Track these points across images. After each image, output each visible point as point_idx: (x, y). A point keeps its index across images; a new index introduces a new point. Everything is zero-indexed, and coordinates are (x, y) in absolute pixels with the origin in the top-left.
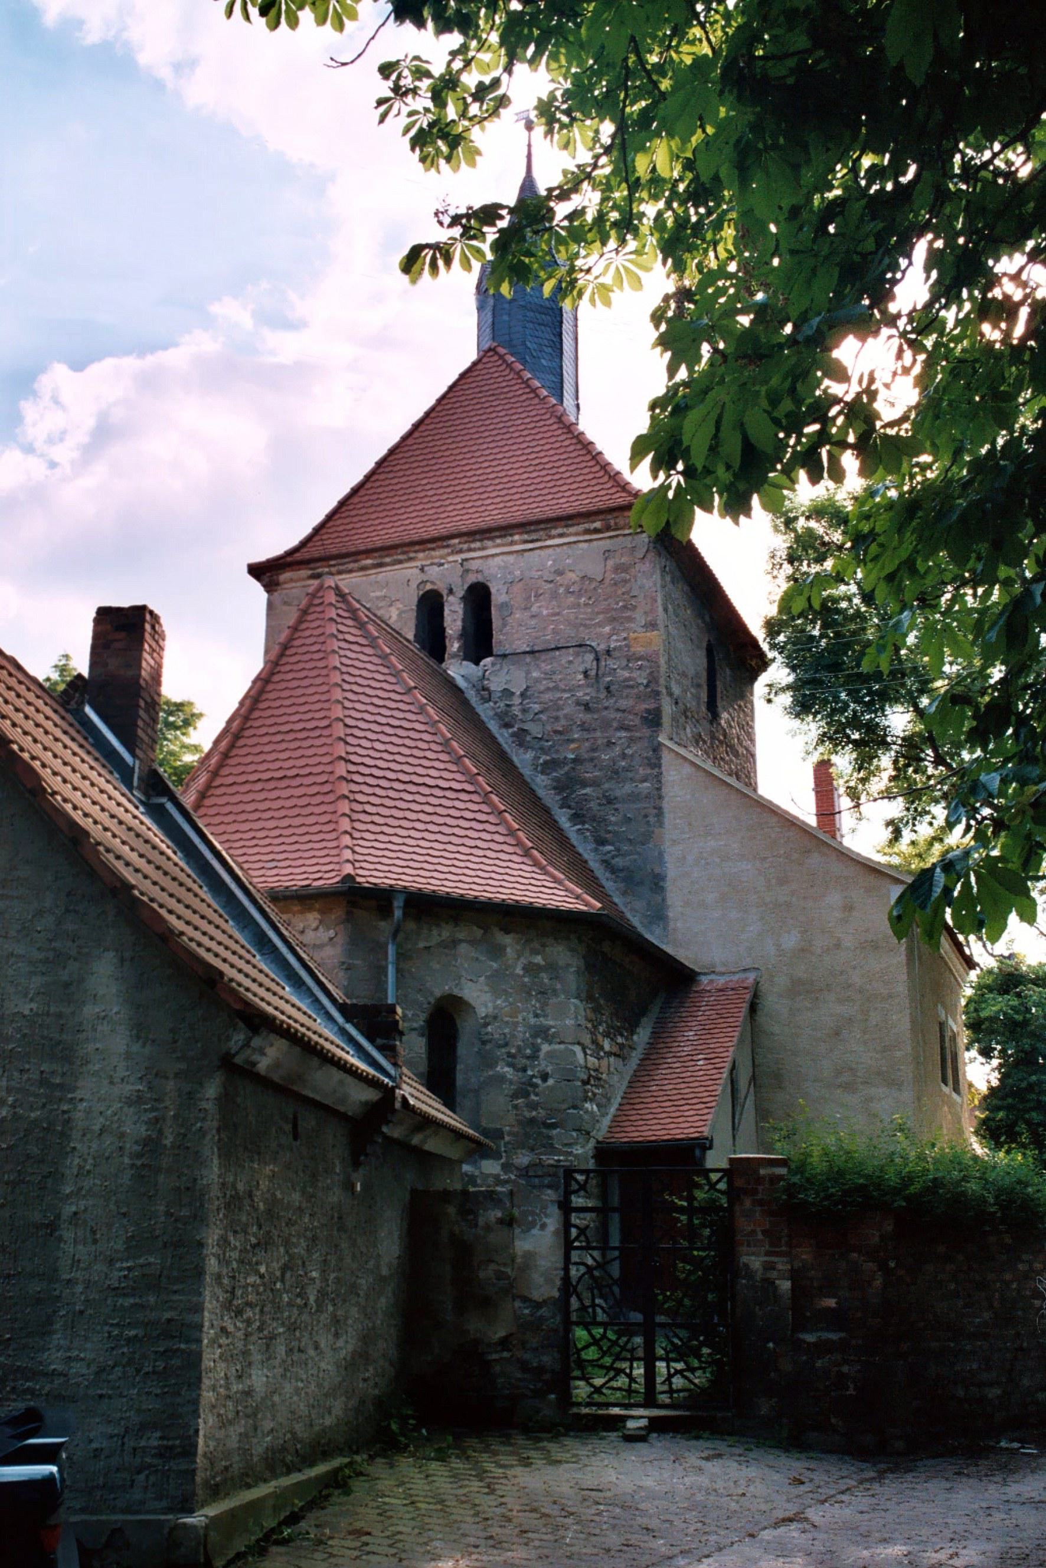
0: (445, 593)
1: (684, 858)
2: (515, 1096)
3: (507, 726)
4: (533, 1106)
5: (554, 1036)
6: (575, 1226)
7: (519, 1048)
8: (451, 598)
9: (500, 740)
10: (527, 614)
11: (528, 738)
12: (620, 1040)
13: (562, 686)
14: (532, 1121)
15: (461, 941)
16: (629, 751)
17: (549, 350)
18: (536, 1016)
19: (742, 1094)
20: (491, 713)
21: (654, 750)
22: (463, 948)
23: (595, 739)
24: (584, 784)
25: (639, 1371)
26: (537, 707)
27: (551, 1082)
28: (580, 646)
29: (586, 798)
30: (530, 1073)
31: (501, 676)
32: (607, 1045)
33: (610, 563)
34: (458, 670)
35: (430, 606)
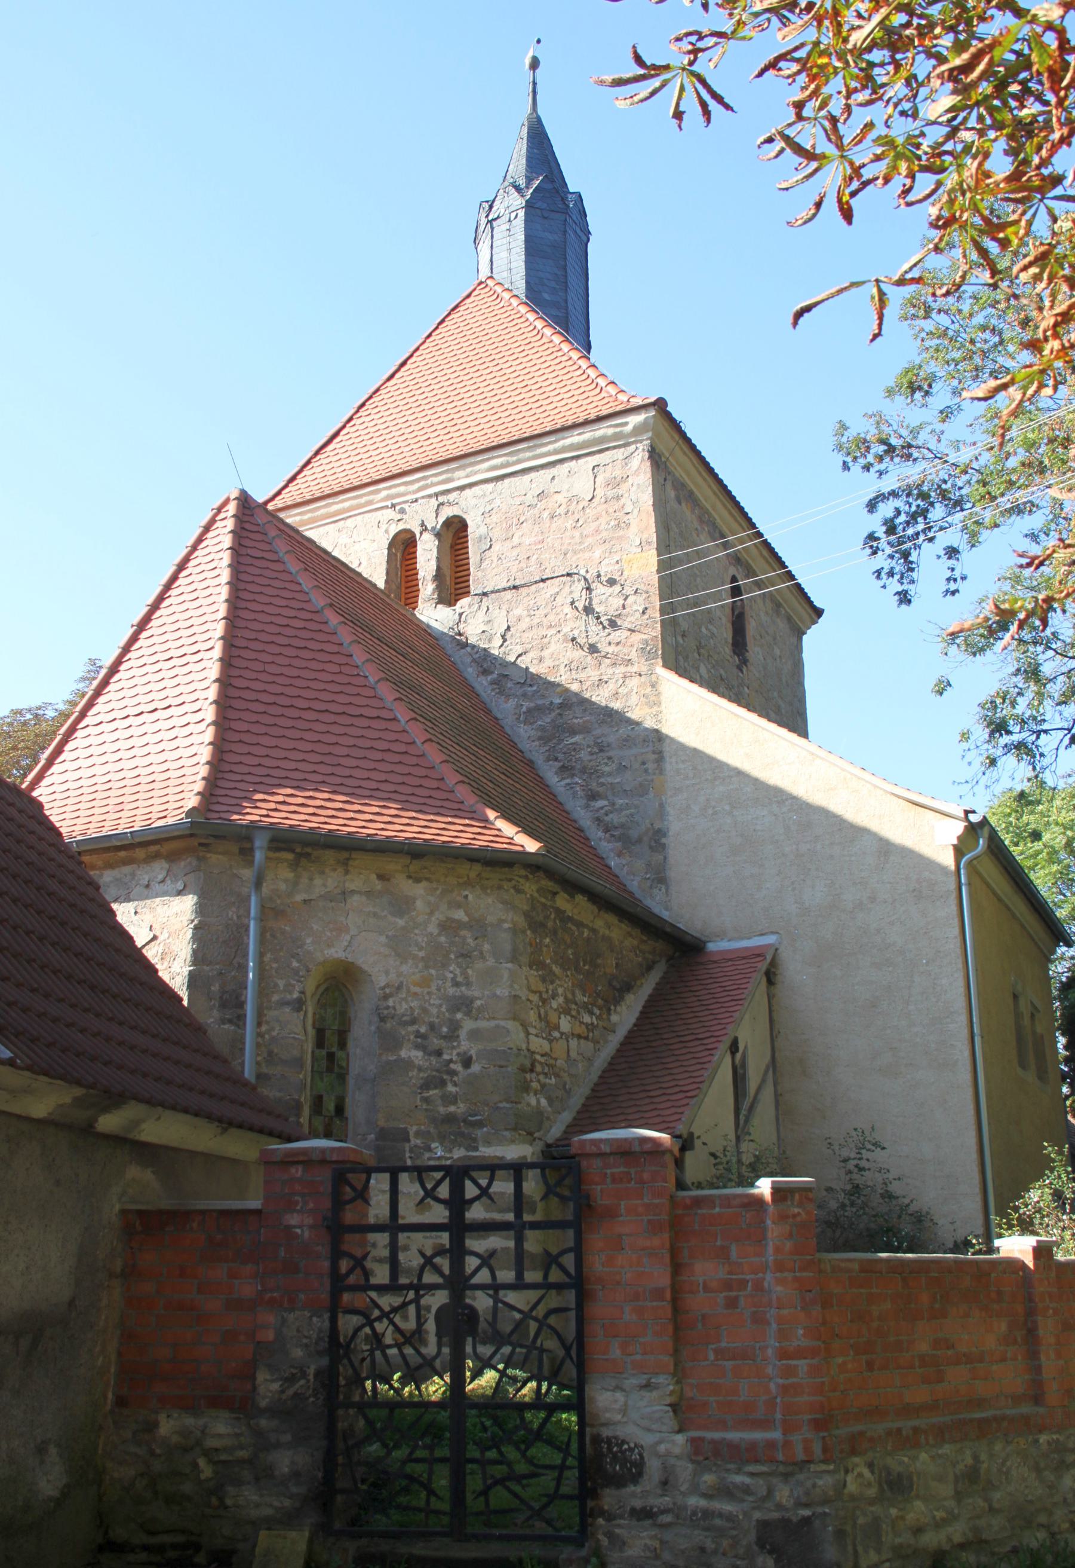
1: (688, 807)
2: (426, 1085)
3: (485, 672)
4: (453, 1100)
5: (480, 1009)
7: (432, 1027)
9: (479, 689)
10: (508, 544)
11: (509, 685)
12: (587, 1019)
14: (450, 1119)
15: (353, 892)
17: (553, 284)
18: (456, 984)
19: (752, 1084)
20: (469, 660)
21: (653, 686)
22: (355, 900)
24: (573, 732)
25: (442, 1481)
27: (475, 1068)
29: (576, 747)
30: (446, 1057)
32: (565, 1024)
35: (403, 547)
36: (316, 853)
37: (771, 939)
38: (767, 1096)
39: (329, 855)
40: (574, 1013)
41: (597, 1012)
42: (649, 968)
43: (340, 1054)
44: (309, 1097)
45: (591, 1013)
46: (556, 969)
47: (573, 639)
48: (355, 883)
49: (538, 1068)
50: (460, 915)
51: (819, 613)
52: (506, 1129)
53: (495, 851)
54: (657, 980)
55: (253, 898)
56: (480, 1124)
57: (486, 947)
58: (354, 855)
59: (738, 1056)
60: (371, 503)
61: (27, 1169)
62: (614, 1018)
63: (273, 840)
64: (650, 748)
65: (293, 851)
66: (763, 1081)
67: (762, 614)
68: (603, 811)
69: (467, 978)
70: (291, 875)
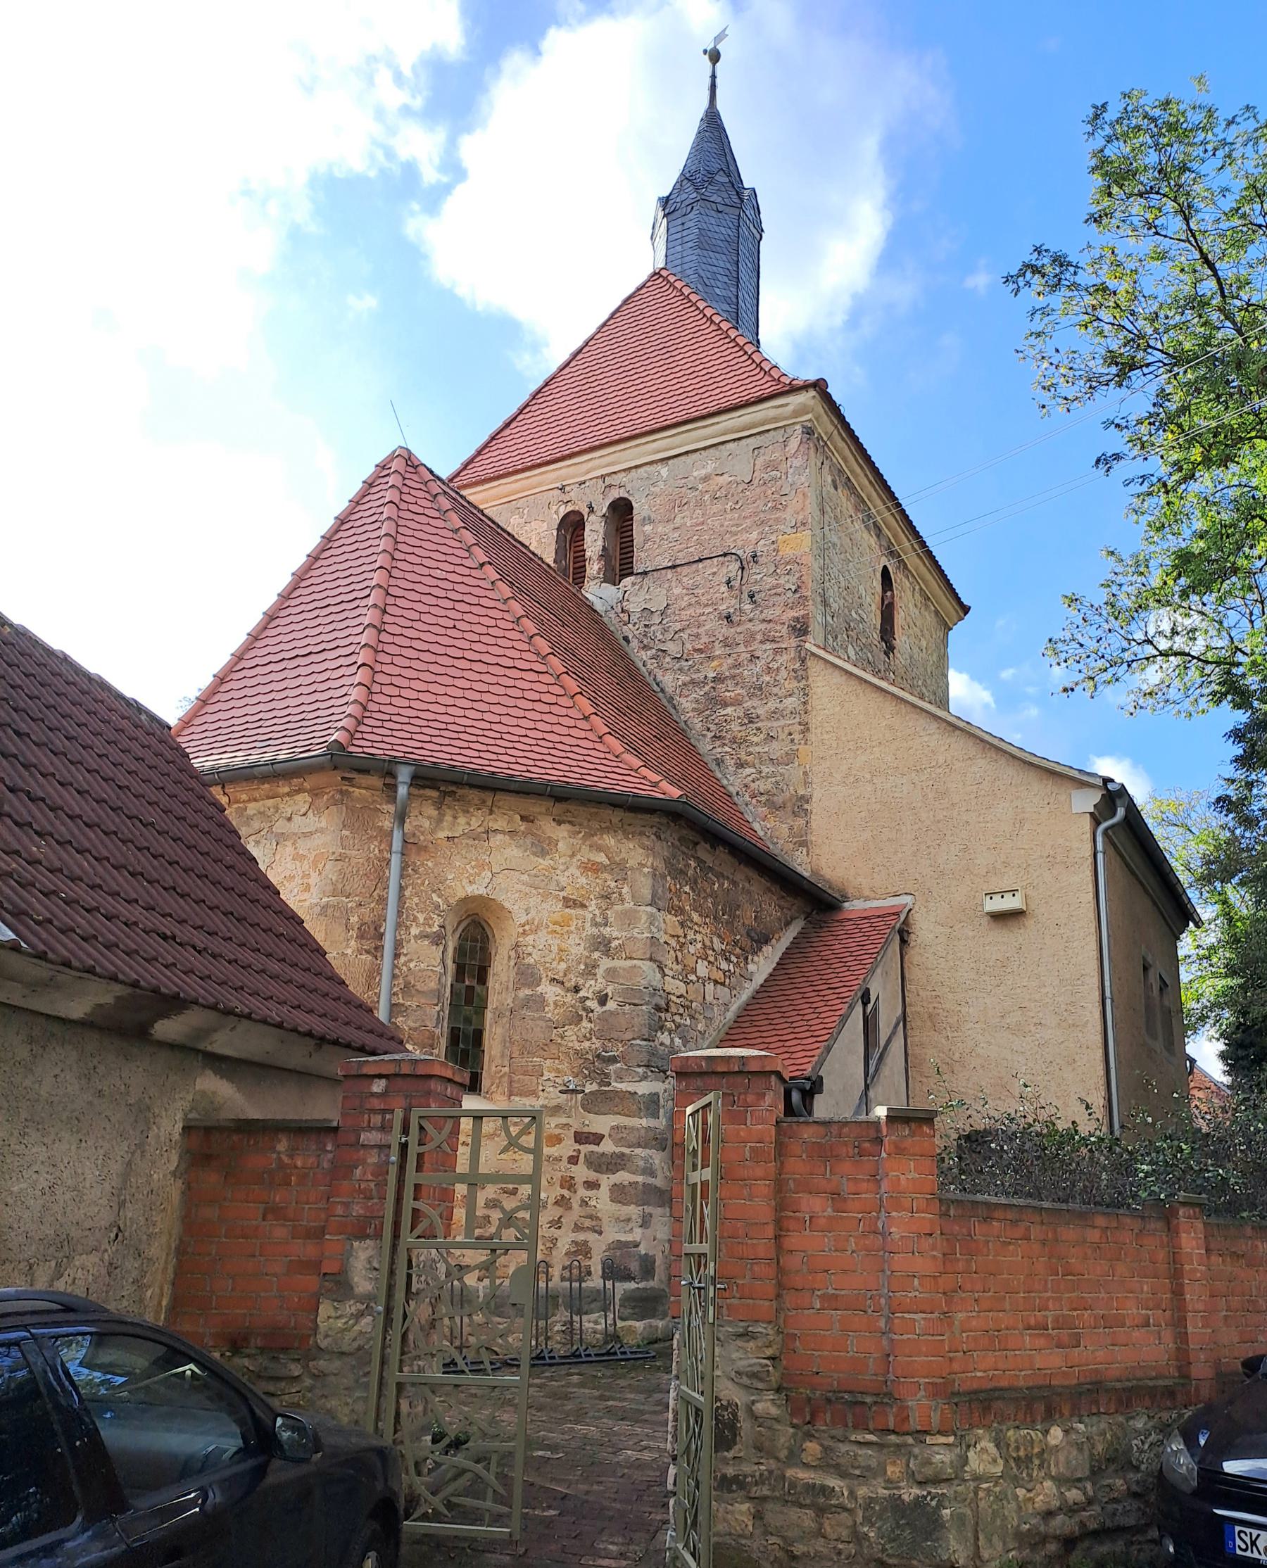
0: (585, 511)
6: (518, 1209)
8: (592, 517)
12: (724, 966)
13: (703, 600)
16: (774, 665)
23: (739, 654)
26: (678, 626)
27: (611, 1005)
28: (725, 555)
31: (637, 595)
32: (702, 969)
33: (760, 462)
34: (598, 593)
35: (572, 526)
36: (460, 792)
37: (907, 900)
38: (897, 1045)
39: (473, 795)
40: (712, 959)
41: (733, 958)
42: (788, 924)
43: (478, 988)
44: (445, 1029)
45: (728, 960)
46: (695, 916)
47: (728, 618)
48: (500, 824)
49: (673, 1009)
50: (601, 858)
51: (966, 610)
52: (639, 1066)
53: (636, 796)
54: (795, 934)
55: (395, 832)
56: (613, 1060)
57: (625, 890)
58: (499, 796)
59: (870, 1007)
60: (540, 485)
61: (56, 1076)
62: (751, 967)
63: (415, 777)
64: (797, 720)
65: (438, 789)
66: (894, 1033)
67: (911, 606)
68: (750, 778)
69: (605, 918)
70: (435, 813)
